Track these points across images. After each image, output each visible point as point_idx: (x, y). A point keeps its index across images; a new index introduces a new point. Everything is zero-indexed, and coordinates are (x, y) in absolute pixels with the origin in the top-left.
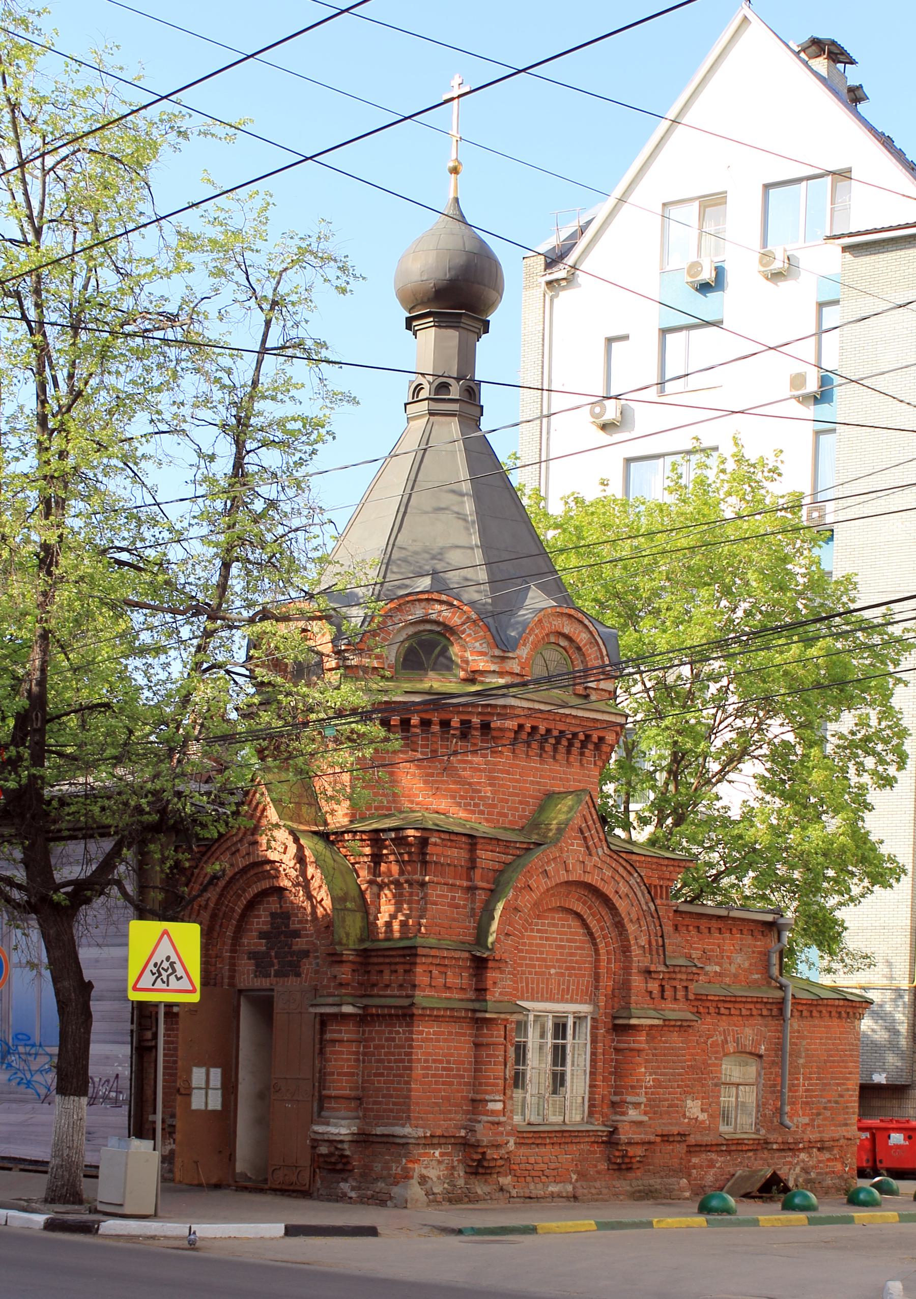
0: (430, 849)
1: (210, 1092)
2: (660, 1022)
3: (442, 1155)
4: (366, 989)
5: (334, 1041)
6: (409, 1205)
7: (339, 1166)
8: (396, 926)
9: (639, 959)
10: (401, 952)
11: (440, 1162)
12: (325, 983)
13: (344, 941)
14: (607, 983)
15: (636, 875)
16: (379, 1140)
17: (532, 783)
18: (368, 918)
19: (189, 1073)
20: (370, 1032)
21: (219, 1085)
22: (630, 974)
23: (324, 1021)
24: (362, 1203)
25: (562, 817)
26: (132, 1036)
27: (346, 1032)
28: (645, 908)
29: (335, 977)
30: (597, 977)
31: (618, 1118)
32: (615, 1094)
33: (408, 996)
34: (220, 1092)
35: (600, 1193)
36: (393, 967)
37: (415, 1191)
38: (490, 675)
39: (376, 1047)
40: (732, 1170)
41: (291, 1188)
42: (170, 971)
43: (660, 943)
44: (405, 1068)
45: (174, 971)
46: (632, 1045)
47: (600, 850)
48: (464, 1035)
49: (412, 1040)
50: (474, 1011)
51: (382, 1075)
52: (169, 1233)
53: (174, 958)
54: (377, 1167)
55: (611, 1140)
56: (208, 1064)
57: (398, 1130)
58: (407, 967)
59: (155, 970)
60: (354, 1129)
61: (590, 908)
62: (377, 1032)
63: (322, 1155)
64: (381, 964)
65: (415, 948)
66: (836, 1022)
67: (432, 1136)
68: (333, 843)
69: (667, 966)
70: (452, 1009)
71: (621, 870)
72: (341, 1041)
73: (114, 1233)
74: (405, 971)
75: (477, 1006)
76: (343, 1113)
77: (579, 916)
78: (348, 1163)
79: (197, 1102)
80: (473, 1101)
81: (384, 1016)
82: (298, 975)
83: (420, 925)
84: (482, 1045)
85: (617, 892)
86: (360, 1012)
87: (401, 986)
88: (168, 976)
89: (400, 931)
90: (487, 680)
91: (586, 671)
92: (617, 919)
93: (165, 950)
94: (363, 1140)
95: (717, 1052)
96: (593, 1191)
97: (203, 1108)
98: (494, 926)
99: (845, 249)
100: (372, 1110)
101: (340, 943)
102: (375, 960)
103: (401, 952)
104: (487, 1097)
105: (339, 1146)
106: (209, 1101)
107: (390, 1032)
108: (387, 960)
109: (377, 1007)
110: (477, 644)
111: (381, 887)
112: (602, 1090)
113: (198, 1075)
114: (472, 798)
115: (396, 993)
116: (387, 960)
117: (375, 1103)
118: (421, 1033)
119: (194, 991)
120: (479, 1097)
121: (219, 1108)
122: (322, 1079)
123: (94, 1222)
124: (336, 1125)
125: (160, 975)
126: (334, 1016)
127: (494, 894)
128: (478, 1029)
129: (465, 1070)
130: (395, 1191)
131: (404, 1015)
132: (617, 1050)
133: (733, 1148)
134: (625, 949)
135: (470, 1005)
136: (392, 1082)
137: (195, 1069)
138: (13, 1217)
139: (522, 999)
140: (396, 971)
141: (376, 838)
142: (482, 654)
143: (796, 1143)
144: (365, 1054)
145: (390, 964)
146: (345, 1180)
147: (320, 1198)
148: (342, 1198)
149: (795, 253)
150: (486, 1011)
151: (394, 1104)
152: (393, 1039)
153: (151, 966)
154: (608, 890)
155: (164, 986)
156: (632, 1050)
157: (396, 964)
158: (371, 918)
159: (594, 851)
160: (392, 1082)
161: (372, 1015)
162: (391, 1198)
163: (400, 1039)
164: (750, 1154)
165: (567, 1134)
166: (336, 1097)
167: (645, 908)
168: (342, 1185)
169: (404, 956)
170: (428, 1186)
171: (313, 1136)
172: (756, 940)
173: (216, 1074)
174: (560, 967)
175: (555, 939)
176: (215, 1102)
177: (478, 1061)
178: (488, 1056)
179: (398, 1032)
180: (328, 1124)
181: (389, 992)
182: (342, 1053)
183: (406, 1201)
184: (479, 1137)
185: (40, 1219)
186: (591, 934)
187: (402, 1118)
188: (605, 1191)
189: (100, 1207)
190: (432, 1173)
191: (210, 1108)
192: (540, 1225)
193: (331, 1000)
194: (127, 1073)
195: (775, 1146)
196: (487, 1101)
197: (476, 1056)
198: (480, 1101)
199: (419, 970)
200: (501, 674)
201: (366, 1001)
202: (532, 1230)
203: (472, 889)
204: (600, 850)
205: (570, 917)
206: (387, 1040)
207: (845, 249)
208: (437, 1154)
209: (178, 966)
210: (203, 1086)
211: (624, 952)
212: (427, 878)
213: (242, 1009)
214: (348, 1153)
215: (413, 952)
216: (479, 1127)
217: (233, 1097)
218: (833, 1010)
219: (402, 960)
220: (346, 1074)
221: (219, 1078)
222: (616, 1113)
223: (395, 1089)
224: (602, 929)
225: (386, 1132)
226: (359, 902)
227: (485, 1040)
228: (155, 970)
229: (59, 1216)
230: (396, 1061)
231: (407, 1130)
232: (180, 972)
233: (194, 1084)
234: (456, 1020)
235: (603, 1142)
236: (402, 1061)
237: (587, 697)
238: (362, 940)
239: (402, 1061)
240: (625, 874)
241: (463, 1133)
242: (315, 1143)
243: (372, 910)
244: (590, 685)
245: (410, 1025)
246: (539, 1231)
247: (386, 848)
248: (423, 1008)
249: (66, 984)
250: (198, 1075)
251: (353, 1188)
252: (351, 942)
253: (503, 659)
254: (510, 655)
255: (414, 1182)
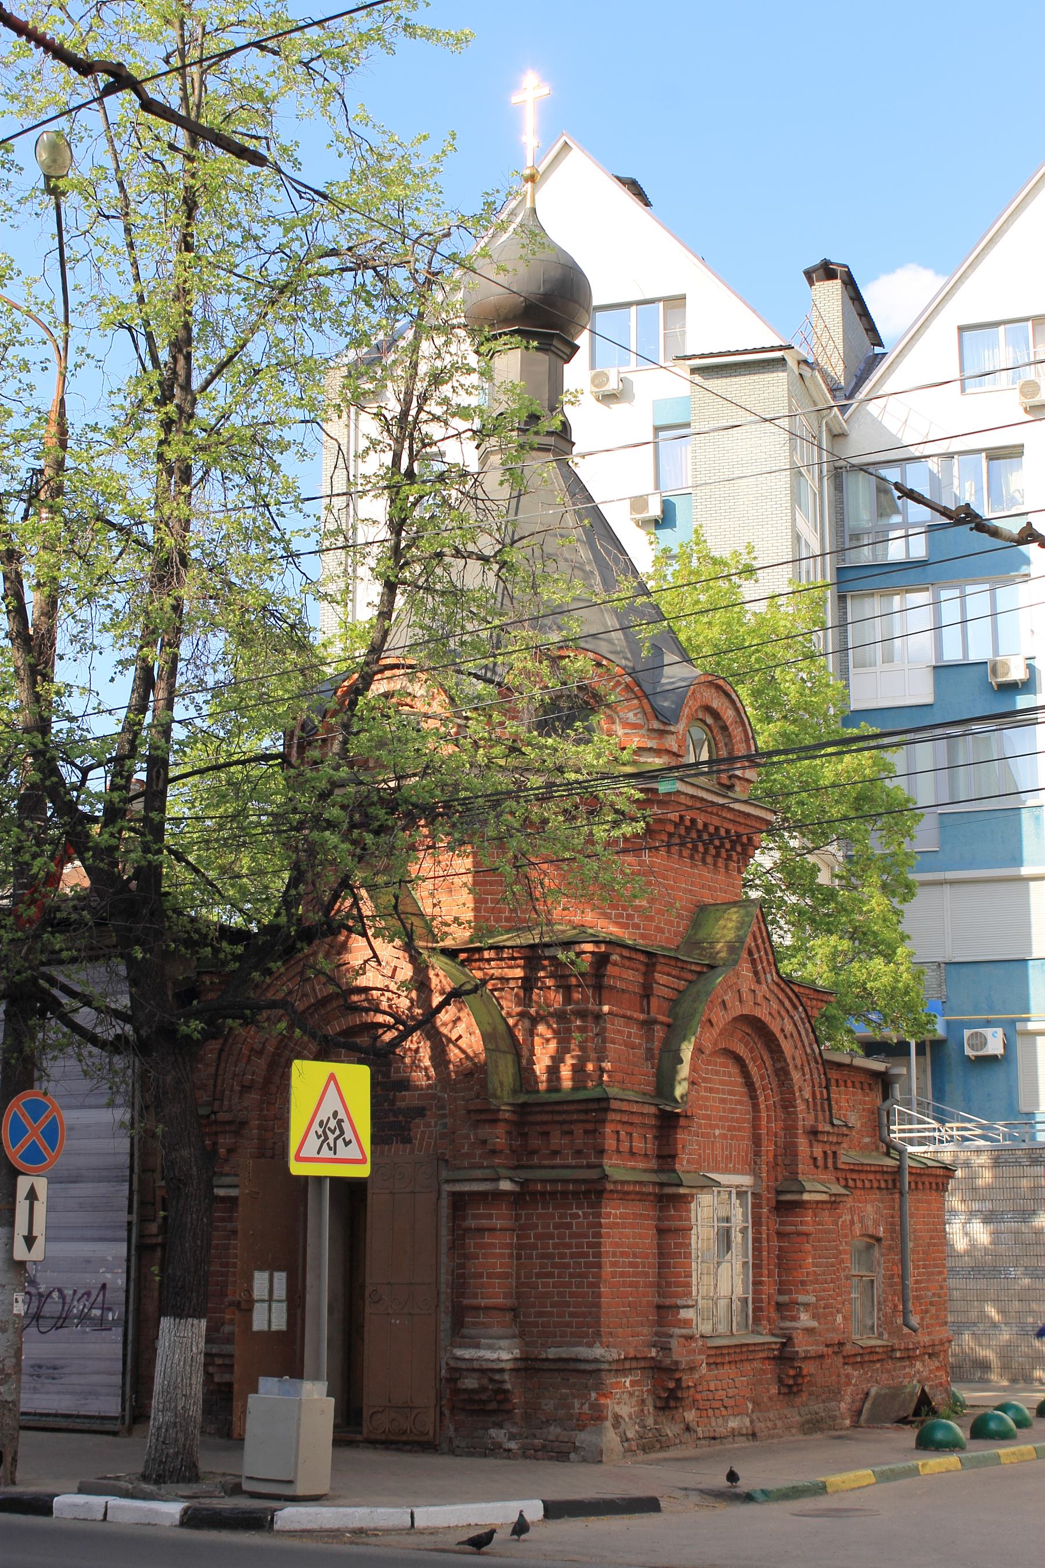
0: (610, 969)
1: (274, 1305)
2: (824, 1197)
3: (633, 1383)
4: (522, 1156)
5: (481, 1230)
6: (604, 1459)
7: (493, 1406)
8: (566, 1072)
9: (804, 1117)
10: (583, 1106)
11: (631, 1394)
12: (465, 1150)
13: (499, 1093)
14: (768, 1148)
15: (801, 1009)
16: (553, 1366)
17: (686, 891)
18: (519, 1062)
19: (250, 1280)
20: (529, 1217)
21: (284, 1296)
22: (796, 1136)
23: (460, 1203)
24: (525, 1456)
25: (730, 935)
26: (129, 1231)
27: (499, 1218)
28: (809, 1051)
29: (484, 1142)
30: (757, 1140)
31: (788, 1324)
32: (780, 1292)
33: (590, 1166)
34: (284, 1305)
35: (775, 1427)
36: (566, 1127)
37: (610, 1438)
38: (645, 754)
39: (536, 1237)
40: (865, 1387)
41: (404, 1438)
42: (337, 1132)
43: (825, 1096)
44: (589, 1265)
45: (342, 1132)
46: (800, 1228)
47: (769, 976)
48: (646, 1217)
49: (600, 1225)
50: (661, 1185)
51: (551, 1275)
52: (382, 1524)
53: (342, 1115)
54: (548, 1405)
55: (784, 1356)
56: (271, 1267)
57: (583, 1352)
58: (590, 1127)
59: (320, 1132)
60: (517, 1353)
61: (752, 1051)
62: (539, 1216)
63: (466, 1390)
64: (546, 1123)
65: (607, 1099)
66: (934, 1193)
67: (626, 1359)
68: (462, 963)
69: (833, 1125)
70: (641, 1183)
71: (787, 1003)
72: (492, 1230)
73: (297, 1527)
74: (586, 1132)
75: (664, 1178)
76: (496, 1330)
77: (739, 1060)
78: (506, 1400)
79: (259, 1323)
80: (659, 1307)
81: (553, 1194)
82: (407, 1140)
83: (602, 1070)
84: (669, 1230)
85: (782, 1030)
86: (517, 1189)
87: (579, 1153)
88: (336, 1139)
89: (573, 1079)
90: (642, 760)
91: (732, 759)
92: (778, 1065)
93: (331, 1103)
94: (529, 1367)
95: (846, 1236)
96: (769, 1424)
97: (265, 1328)
98: (684, 1071)
99: (694, 371)
100: (536, 1324)
101: (495, 1096)
102: (539, 1118)
103: (583, 1106)
104: (679, 1302)
105: (497, 1377)
106: (273, 1319)
107: (562, 1216)
108: (557, 1118)
109: (544, 1181)
110: (631, 715)
111: (535, 1021)
112: (769, 1288)
113: (260, 1280)
114: (624, 908)
115: (570, 1161)
116: (557, 1118)
117: (540, 1314)
118: (608, 1215)
119: (363, 1161)
120: (668, 1302)
121: (284, 1328)
122: (460, 1283)
123: (264, 1510)
124: (490, 1347)
125: (326, 1138)
126: (483, 1195)
127: (675, 1032)
128: (661, 1209)
129: (650, 1266)
130: (582, 1438)
131: (587, 1193)
132: (780, 1235)
133: (867, 1358)
134: (787, 1104)
135: (653, 1178)
136: (569, 1285)
137: (257, 1275)
138: (115, 1507)
139: (717, 1170)
140: (571, 1133)
141: (532, 957)
142: (635, 726)
143: (914, 1349)
144: (520, 1247)
145: (561, 1123)
146: (499, 1425)
147: (453, 1452)
148: (494, 1450)
149: (628, 375)
150: (680, 1185)
151: (572, 1315)
152: (569, 1226)
153: (315, 1126)
154: (775, 1027)
155: (330, 1154)
156: (799, 1234)
157: (571, 1122)
158: (524, 1062)
159: (762, 976)
160: (569, 1285)
161: (533, 1194)
162: (575, 1449)
163: (580, 1225)
164: (878, 1365)
165: (744, 1349)
166: (487, 1308)
167: (809, 1051)
168: (493, 1432)
169: (587, 1112)
170: (621, 1429)
171: (452, 1363)
172: (865, 1095)
173: (280, 1278)
174: (723, 1127)
175: (717, 1091)
176: (279, 1322)
177: (662, 1253)
178: (676, 1246)
179: (577, 1216)
180: (477, 1346)
181: (558, 1161)
182: (493, 1246)
183: (601, 1452)
184: (675, 1357)
185: (172, 1509)
186: (749, 1084)
187: (587, 1335)
188: (779, 1423)
189: (247, 1486)
190: (625, 1410)
191: (274, 1328)
192: (834, 1480)
193: (478, 1173)
194: (121, 1281)
195: (898, 1355)
196: (679, 1307)
197: (660, 1246)
198: (670, 1307)
199: (608, 1130)
200: (658, 752)
201: (524, 1174)
202: (820, 1489)
203: (648, 1024)
204: (769, 976)
205: (730, 1062)
206: (557, 1226)
207: (694, 371)
208: (628, 1384)
209: (346, 1125)
210: (266, 1297)
211: (785, 1108)
212: (606, 1008)
213: (310, 1189)
214: (508, 1386)
215: (603, 1105)
216: (674, 1343)
217: (299, 1311)
218: (933, 1180)
219: (583, 1117)
220: (500, 1276)
221: (284, 1286)
222: (783, 1318)
223: (572, 1294)
224: (762, 1078)
225: (564, 1356)
226: (509, 1041)
227: (674, 1224)
228: (320, 1132)
229: (195, 1503)
230: (572, 1256)
231: (598, 1352)
232: (349, 1135)
233: (256, 1295)
234: (642, 1197)
235: (774, 1358)
236: (586, 1255)
237: (731, 787)
238: (515, 1092)
239: (586, 1255)
240: (790, 1008)
241: (653, 1353)
242: (456, 1373)
243: (525, 1052)
244: (738, 773)
245: (598, 1205)
246: (829, 1490)
247: (544, 968)
248: (615, 1182)
249: (185, 1153)
250: (260, 1280)
251: (512, 1437)
252: (505, 1093)
253: (662, 733)
254: (672, 728)
255: (608, 1424)
